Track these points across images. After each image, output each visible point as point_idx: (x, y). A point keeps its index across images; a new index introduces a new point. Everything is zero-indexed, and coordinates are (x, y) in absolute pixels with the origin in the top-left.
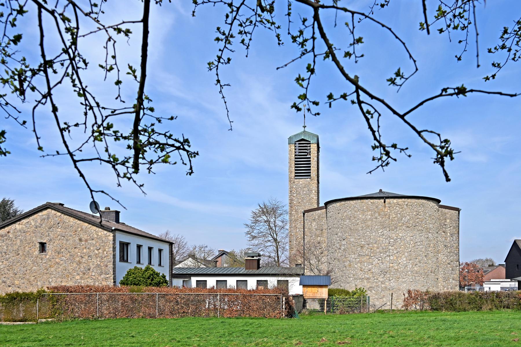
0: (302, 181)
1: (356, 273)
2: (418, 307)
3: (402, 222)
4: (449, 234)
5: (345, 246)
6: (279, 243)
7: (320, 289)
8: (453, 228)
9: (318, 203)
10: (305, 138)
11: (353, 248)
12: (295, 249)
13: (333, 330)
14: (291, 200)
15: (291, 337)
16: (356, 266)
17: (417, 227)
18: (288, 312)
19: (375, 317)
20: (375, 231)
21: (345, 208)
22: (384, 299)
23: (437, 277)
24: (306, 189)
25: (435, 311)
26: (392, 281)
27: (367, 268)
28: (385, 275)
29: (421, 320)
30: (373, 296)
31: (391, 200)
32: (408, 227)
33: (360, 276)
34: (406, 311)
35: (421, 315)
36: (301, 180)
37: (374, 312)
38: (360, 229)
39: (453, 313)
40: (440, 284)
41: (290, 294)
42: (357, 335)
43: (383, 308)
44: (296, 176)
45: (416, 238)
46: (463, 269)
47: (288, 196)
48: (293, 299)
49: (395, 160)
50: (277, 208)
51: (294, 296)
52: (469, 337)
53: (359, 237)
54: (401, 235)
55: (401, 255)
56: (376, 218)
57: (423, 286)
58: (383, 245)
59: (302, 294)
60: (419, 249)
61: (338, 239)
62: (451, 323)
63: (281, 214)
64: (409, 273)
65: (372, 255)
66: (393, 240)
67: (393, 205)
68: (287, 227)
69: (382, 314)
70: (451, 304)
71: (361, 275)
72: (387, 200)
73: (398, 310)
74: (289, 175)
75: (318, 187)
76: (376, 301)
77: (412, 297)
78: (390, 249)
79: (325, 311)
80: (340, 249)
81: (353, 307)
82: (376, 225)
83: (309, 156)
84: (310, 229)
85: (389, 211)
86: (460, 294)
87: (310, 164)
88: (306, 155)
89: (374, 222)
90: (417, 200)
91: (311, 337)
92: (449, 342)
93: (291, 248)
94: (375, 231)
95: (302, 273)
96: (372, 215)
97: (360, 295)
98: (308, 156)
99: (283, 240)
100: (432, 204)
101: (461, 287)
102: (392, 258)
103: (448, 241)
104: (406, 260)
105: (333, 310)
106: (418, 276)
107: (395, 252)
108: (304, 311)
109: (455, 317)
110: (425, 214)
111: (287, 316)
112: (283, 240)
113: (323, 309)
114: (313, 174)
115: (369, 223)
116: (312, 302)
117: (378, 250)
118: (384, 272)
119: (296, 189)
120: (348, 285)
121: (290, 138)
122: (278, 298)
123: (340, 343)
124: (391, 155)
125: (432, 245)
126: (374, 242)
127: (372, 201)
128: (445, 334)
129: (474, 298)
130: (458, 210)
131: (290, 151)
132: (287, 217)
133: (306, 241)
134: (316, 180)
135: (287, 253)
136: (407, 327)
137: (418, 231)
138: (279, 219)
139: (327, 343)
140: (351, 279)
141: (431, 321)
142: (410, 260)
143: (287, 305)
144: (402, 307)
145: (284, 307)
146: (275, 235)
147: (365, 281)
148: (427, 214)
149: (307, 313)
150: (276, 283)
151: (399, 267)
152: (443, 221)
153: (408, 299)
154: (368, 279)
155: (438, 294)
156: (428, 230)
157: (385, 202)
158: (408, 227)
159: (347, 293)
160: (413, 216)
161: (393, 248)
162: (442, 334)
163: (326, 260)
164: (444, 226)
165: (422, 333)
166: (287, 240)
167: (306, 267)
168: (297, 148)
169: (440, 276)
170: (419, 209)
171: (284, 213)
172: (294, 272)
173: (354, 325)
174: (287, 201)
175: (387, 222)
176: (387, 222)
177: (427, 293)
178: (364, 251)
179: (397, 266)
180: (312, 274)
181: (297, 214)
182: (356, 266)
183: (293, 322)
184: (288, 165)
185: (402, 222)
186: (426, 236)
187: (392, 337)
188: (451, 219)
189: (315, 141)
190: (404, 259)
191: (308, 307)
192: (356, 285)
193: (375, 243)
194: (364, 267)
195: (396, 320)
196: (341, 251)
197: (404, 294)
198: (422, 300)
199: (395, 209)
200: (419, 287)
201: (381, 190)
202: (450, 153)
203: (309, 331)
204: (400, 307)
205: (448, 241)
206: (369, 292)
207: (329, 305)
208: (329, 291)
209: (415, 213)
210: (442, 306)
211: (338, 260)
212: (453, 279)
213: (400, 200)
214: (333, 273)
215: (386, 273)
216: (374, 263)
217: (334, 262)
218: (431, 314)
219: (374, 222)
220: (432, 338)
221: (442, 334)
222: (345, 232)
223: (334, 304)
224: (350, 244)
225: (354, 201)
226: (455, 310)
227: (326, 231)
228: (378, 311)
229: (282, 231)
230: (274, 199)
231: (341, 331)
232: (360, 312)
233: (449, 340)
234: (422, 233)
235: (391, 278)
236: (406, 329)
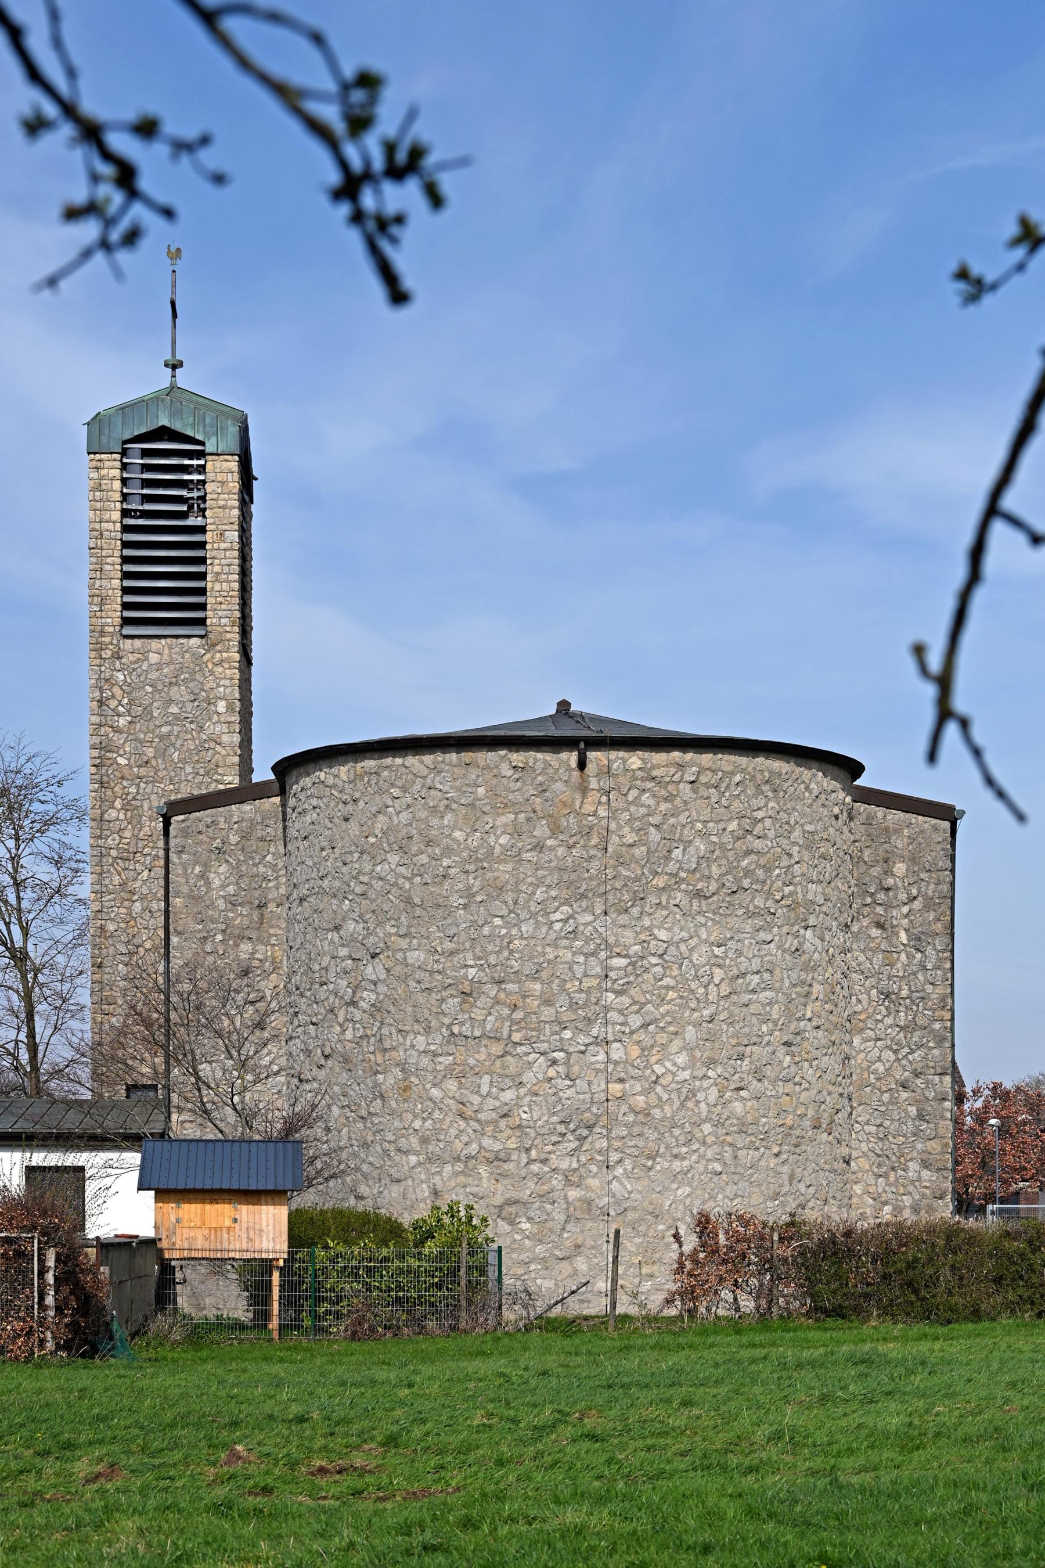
0: (160, 652)
1: (437, 1131)
2: (747, 1304)
3: (672, 867)
4: (903, 937)
5: (382, 988)
6: (37, 971)
7: (245, 1211)
8: (927, 907)
9: (246, 766)
10: (177, 426)
11: (421, 999)
12: (120, 1008)
13: (295, 1409)
14: (103, 749)
15: (69, 1446)
16: (435, 1092)
17: (746, 897)
18: (73, 1327)
19: (525, 1349)
20: (533, 915)
21: (381, 792)
22: (581, 1264)
23: (844, 1151)
24: (179, 693)
25: (830, 1322)
26: (619, 1171)
27: (491, 1103)
28: (582, 1139)
29: (754, 1361)
30: (521, 1249)
31: (614, 754)
32: (699, 894)
33: (458, 1145)
34: (686, 1321)
35: (758, 1338)
36: (155, 644)
37: (528, 1329)
38: (457, 901)
39: (917, 1329)
40: (858, 1189)
41: (91, 1233)
42: (417, 1432)
43: (575, 1308)
44: (126, 621)
45: (739, 953)
46: (981, 1118)
47: (88, 729)
48: (100, 1262)
49: (168, 213)
50: (30, 787)
51: (106, 1247)
52: (972, 1430)
53: (449, 945)
54: (663, 935)
55: (662, 1038)
56: (539, 847)
57: (776, 1196)
58: (572, 986)
59: (151, 1233)
60: (754, 1008)
61: (343, 952)
62: (901, 1370)
63: (49, 822)
64: (707, 1128)
65: (516, 1037)
66: (622, 962)
67: (624, 781)
68: (83, 888)
69: (566, 1335)
70: (909, 1284)
71: (460, 1136)
72: (592, 755)
73: (651, 1320)
74: (93, 615)
75: (245, 684)
76: (543, 1267)
77: (721, 1249)
78: (607, 1009)
79: (274, 1324)
80: (353, 1003)
81: (419, 1301)
82: (540, 882)
83: (199, 521)
84: (197, 899)
85: (602, 812)
86: (951, 1233)
87: (202, 561)
88: (183, 515)
89: (527, 869)
90: (743, 761)
91: (175, 1445)
92: (874, 1457)
93: (102, 1002)
94: (533, 915)
95: (158, 1128)
96: (516, 832)
97: (456, 1241)
98: (191, 521)
99: (61, 959)
100: (818, 780)
101: (964, 1205)
102: (617, 1052)
103: (899, 970)
104: (692, 1065)
105: (317, 1317)
106: (752, 1147)
107: (636, 1021)
108: (161, 1322)
109: (924, 1346)
110: (786, 830)
111: (67, 1346)
112: (61, 959)
113: (263, 1315)
114: (221, 613)
115: (504, 871)
116: (211, 1284)
117: (548, 1013)
118: (579, 1126)
119: (129, 689)
120: (395, 1190)
121: (97, 424)
122: (20, 1254)
123: (322, 1470)
124: (145, 183)
125: (817, 989)
126: (529, 968)
127: (517, 757)
128: (857, 1418)
129: (1022, 1255)
130: (949, 815)
131: (99, 488)
132: (80, 838)
133: (176, 962)
134: (235, 644)
135: (82, 1029)
136: (679, 1393)
137: (751, 915)
138: (40, 844)
139: (252, 1468)
140: (413, 1159)
141: (800, 1366)
142: (711, 1063)
143: (66, 1290)
144: (669, 1302)
145: (50, 1300)
146: (16, 930)
147: (483, 1170)
148: (797, 833)
149: (176, 1336)
150: (16, 1182)
151: (653, 1099)
152: (875, 871)
153: (696, 1262)
154: (498, 1158)
155: (848, 1234)
156: (800, 913)
157: (582, 765)
158: (699, 894)
159: (391, 1231)
160: (726, 838)
161: (625, 1000)
162: (844, 1423)
163: (283, 1061)
164: (881, 896)
165: (746, 1418)
166: (83, 956)
167: (175, 1097)
168: (134, 475)
169: (862, 1146)
170: (755, 803)
171: (66, 814)
172: (112, 1124)
173: (410, 1386)
174: (83, 757)
175: (594, 866)
176: (594, 866)
177: (793, 1228)
178: (478, 1014)
179: (646, 1092)
180: (211, 1134)
181: (135, 821)
182: (435, 1092)
183: (99, 1380)
184: (86, 563)
185: (672, 867)
186: (792, 943)
187: (593, 1437)
188: (913, 860)
189: (230, 441)
190: (682, 1059)
191: (183, 1301)
192: (436, 1193)
193: (535, 977)
194: (476, 1099)
195: (632, 1362)
196: (358, 1015)
197: (677, 1237)
198: (767, 1264)
199: (636, 802)
200: (756, 1199)
201: (564, 706)
202: (405, 164)
203: (169, 1416)
204: (655, 1302)
205: (899, 970)
206: (503, 1226)
207: (294, 1295)
208: (295, 1220)
209: (733, 826)
210: (866, 1296)
211: (346, 1060)
212: (925, 1164)
213: (659, 758)
214: (318, 1131)
215: (590, 1127)
216: (528, 1077)
217: (322, 1074)
218: (811, 1335)
219: (527, 869)
220: (793, 1440)
221: (844, 1423)
222: (381, 917)
223: (319, 1286)
224: (404, 979)
225: (428, 759)
226: (927, 1314)
227: (282, 911)
228: (546, 1325)
229: (55, 910)
230: (11, 740)
231: (340, 1413)
232: (454, 1328)
233: (872, 1447)
234: (767, 927)
235: (614, 1157)
236: (668, 1401)
